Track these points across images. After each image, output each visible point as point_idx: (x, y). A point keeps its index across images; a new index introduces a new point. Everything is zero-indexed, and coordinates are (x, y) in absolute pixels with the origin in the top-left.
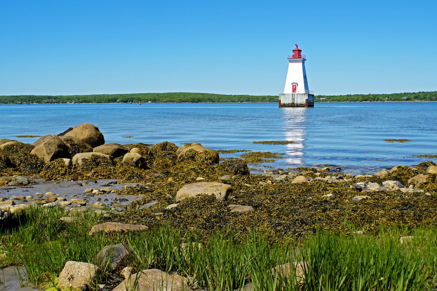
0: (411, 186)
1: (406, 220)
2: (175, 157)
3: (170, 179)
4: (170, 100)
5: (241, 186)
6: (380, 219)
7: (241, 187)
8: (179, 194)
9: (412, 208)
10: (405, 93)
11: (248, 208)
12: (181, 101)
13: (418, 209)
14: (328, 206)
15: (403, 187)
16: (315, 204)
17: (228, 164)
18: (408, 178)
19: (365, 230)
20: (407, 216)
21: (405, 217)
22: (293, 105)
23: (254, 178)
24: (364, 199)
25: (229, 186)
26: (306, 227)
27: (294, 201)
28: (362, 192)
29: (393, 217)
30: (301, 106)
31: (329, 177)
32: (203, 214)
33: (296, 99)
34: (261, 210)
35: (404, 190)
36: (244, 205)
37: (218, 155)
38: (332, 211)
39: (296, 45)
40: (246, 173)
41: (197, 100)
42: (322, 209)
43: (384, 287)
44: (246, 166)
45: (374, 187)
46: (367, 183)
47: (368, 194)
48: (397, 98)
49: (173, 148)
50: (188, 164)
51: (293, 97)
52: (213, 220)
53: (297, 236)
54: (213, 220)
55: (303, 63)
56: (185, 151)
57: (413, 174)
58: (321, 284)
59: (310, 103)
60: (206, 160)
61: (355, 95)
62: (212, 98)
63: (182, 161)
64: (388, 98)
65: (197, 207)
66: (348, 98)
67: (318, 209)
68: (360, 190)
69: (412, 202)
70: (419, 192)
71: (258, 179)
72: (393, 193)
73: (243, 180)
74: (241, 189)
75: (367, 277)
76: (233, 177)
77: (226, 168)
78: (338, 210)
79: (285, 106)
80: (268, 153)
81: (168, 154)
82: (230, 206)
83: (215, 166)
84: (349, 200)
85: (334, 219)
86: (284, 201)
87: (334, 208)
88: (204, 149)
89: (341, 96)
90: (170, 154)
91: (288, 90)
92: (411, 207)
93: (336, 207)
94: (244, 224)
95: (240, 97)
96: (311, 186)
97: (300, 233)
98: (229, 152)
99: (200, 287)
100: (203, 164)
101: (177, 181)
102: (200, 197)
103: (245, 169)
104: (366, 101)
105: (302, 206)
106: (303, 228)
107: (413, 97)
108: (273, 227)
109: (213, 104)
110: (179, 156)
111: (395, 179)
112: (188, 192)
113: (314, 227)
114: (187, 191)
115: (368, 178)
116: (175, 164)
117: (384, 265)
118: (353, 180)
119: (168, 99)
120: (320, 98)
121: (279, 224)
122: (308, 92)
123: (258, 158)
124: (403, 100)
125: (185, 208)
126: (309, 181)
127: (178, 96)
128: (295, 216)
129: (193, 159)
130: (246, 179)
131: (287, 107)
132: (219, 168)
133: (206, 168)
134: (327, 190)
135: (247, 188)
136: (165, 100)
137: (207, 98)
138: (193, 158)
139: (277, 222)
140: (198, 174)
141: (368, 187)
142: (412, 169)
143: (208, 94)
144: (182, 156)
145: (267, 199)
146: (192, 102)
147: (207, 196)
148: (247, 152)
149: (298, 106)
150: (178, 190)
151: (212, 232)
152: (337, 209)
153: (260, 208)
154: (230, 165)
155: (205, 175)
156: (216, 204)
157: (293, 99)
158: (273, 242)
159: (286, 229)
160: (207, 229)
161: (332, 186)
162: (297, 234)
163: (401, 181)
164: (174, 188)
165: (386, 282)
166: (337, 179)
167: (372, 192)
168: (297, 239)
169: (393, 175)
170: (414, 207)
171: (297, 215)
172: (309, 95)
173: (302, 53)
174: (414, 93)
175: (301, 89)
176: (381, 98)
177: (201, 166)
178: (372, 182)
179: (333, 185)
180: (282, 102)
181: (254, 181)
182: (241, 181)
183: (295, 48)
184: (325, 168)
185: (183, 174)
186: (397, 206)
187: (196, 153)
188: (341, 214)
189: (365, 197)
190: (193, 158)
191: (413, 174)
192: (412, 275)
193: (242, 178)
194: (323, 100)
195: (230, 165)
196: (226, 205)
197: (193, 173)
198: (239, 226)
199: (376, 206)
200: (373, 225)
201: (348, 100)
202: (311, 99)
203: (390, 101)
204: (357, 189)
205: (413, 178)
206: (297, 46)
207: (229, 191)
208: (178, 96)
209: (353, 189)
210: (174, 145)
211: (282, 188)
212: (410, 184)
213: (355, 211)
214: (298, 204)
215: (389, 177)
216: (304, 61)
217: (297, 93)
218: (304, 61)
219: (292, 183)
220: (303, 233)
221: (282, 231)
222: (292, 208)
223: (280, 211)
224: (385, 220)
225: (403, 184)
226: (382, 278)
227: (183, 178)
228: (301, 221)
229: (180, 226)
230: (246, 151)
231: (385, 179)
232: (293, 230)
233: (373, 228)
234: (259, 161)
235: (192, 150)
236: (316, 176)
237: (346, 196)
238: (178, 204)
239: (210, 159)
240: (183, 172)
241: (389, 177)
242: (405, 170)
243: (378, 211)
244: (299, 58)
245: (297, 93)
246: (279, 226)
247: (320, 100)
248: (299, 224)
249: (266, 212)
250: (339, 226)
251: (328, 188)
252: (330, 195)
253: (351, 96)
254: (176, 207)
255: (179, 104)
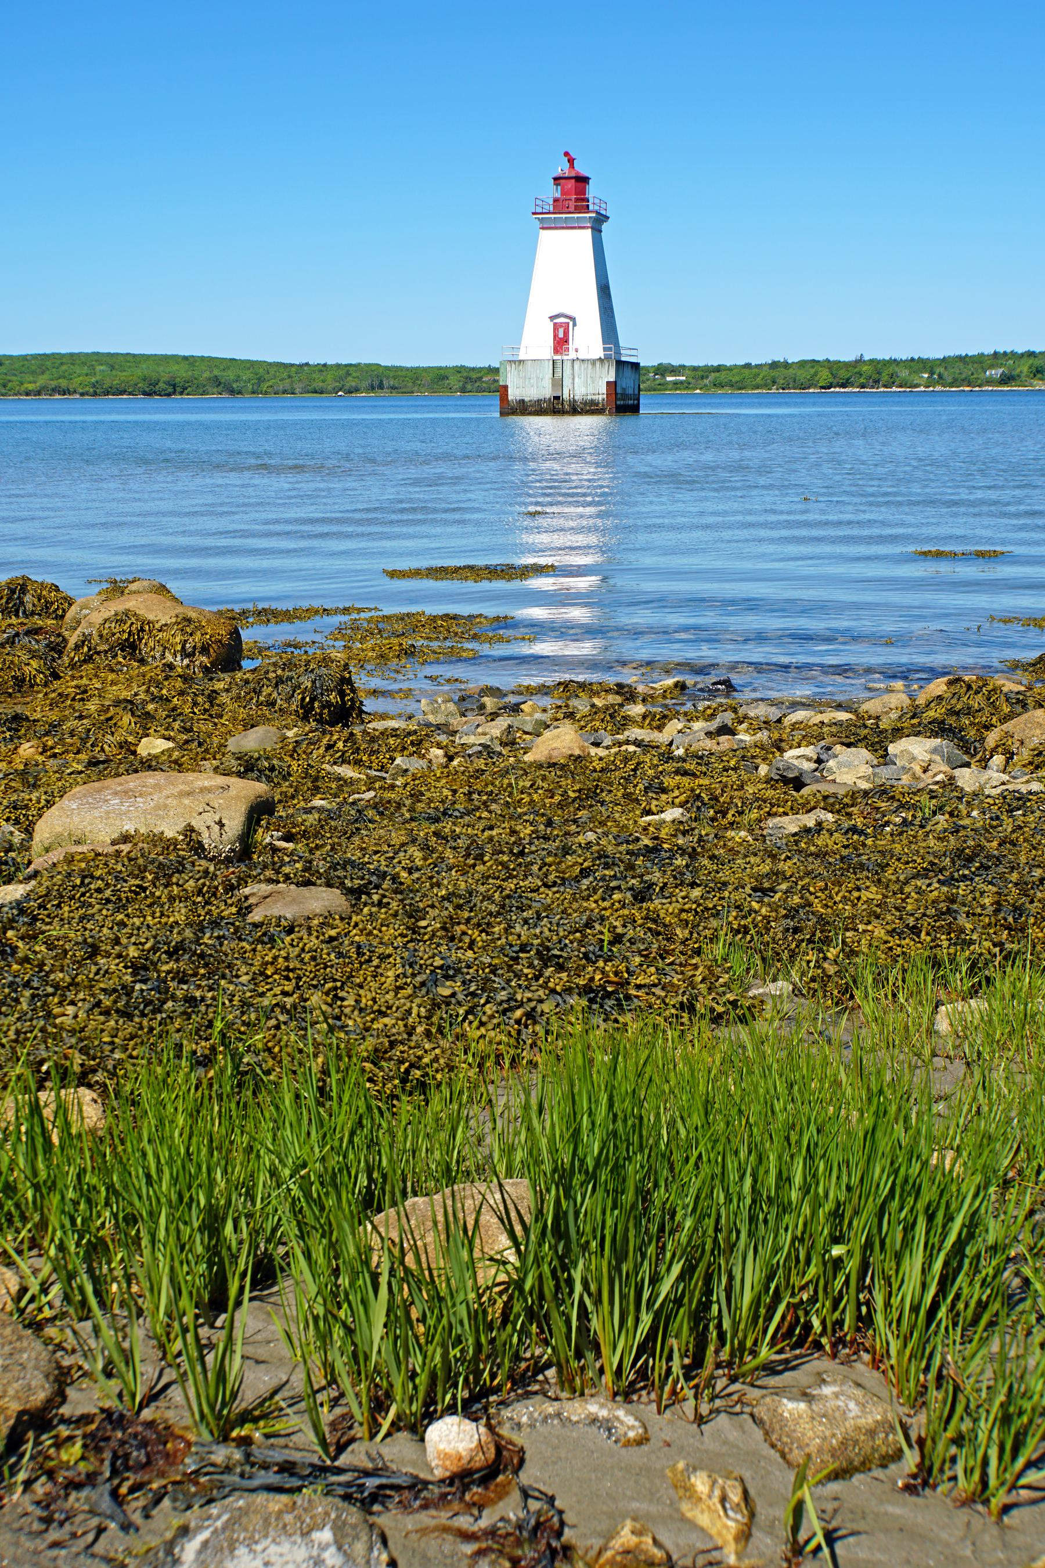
0: (998, 760)
1: (962, 930)
2: (58, 648)
3: (27, 750)
4: (54, 383)
5: (316, 779)
6: (861, 927)
7: (316, 783)
8: (45, 830)
9: (992, 874)
10: (325, 365)
11: (324, 900)
12: (100, 391)
13: (1014, 877)
14: (656, 876)
15: (967, 765)
16: (607, 866)
17: (272, 675)
18: (988, 727)
19: (803, 974)
20: (968, 914)
21: (962, 920)
22: (556, 407)
23: (373, 739)
24: (807, 830)
25: (258, 788)
26: (559, 980)
27: (522, 853)
28: (805, 791)
29: (911, 921)
30: (589, 408)
31: (680, 726)
32: (124, 941)
33: (567, 382)
34: (380, 904)
35: (967, 779)
36: (308, 883)
37: (235, 635)
38: (672, 895)
39: (566, 154)
40: (345, 712)
41: (168, 383)
42: (631, 889)
43: (847, 1282)
44: (349, 681)
45: (851, 769)
46: (829, 749)
47: (828, 802)
48: (966, 373)
49: (54, 604)
50: (111, 676)
51: (558, 375)
52: (165, 968)
53: (518, 1022)
54: (165, 968)
55: (597, 230)
56: (97, 618)
57: (1006, 709)
58: (578, 1288)
59: (625, 396)
60: (188, 656)
61: (803, 364)
62: (230, 375)
63: (88, 659)
64: (932, 373)
65: (108, 901)
66: (774, 373)
67: (619, 888)
68: (798, 783)
69: (995, 844)
70: (1024, 789)
71: (391, 741)
72: (924, 798)
73: (329, 747)
74: (316, 790)
75: (776, 1251)
76: (290, 734)
77: (266, 691)
78: (696, 893)
79: (523, 408)
80: (446, 617)
81: (28, 633)
82: (247, 891)
83: (220, 686)
84: (751, 831)
85: (678, 931)
86: (480, 857)
87: (682, 884)
88: (179, 610)
89: (748, 366)
90: (36, 631)
91: (536, 342)
92: (987, 868)
93: (688, 877)
94: (299, 978)
95: (342, 372)
96: (602, 770)
97: (534, 1009)
98: (288, 616)
99: (72, 1311)
100: (167, 678)
101: (55, 756)
102: (125, 848)
103: (342, 694)
104: (843, 386)
105: (551, 877)
106: (545, 986)
107: (1025, 369)
108: (423, 984)
109: (238, 402)
110: (72, 641)
111: (939, 729)
112: (89, 818)
113: (592, 979)
114: (76, 819)
115: (834, 729)
116: (56, 676)
117: (849, 1188)
118: (776, 736)
119: (42, 381)
120: (663, 375)
121: (449, 972)
122: (618, 352)
123: (407, 640)
124: (989, 382)
125: (59, 906)
126: (597, 744)
127: (86, 370)
128: (518, 928)
129: (132, 655)
130: (340, 745)
131: (530, 414)
132: (235, 691)
133: (182, 693)
134: (664, 791)
135: (340, 788)
136: (31, 387)
137: (207, 375)
138: (130, 647)
139: (438, 962)
140: (145, 721)
141: (830, 770)
142: (1005, 689)
143: (211, 359)
144: (85, 639)
145: (414, 841)
146: (145, 393)
147: (156, 839)
148: (363, 615)
149: (576, 409)
150: (49, 804)
151: (151, 1029)
152: (693, 885)
153: (376, 898)
154: (280, 681)
155: (176, 725)
156: (191, 882)
157: (558, 383)
158: (412, 1066)
159: (473, 994)
160: (130, 1017)
161: (686, 773)
162: (518, 1013)
163: (961, 739)
164: (34, 796)
165: (852, 1265)
166: (709, 734)
167: (842, 792)
168: (519, 1032)
169: (931, 713)
170: (1001, 869)
171: (526, 921)
172: (620, 364)
173: (592, 191)
174: (1031, 354)
175: (588, 340)
176: (904, 373)
177: (159, 685)
178: (848, 745)
179: (691, 766)
180: (513, 395)
181: (373, 752)
182: (321, 751)
183: (562, 168)
184: (670, 682)
185: (81, 726)
186: (932, 864)
187: (145, 627)
188: (707, 909)
189: (810, 820)
190: (130, 647)
191: (1006, 709)
192: (963, 1225)
193: (325, 741)
194: (675, 383)
195: (280, 681)
196: (230, 888)
197: (127, 718)
198: (277, 990)
199: (850, 865)
200: (832, 953)
201: (774, 382)
202: (628, 383)
203: (938, 388)
204: (785, 780)
205: (1004, 727)
206: (571, 161)
207: (259, 811)
208: (86, 370)
209: (768, 780)
210: (57, 589)
211: (486, 778)
212: (994, 751)
213: (765, 892)
214: (535, 868)
215: (911, 721)
216: (598, 223)
217: (572, 355)
218: (598, 223)
219: (528, 758)
220: (546, 1007)
221: (459, 1003)
222: (511, 885)
223: (459, 907)
224: (880, 933)
225: (967, 752)
226: (837, 1251)
227: (84, 741)
228: (538, 952)
229: (17, 1001)
230: (360, 610)
231: (897, 733)
232: (503, 995)
233: (831, 970)
234: (410, 652)
235: (127, 613)
236: (627, 721)
237: (741, 813)
238: (33, 883)
239: (205, 650)
240: (81, 717)
241: (915, 721)
242: (977, 693)
243: (858, 889)
244: (578, 210)
245: (572, 355)
246: (447, 977)
247: (664, 385)
248: (531, 966)
249: (395, 915)
250: (696, 967)
251: (668, 781)
252: (673, 814)
253: (786, 365)
254: (18, 903)
255: (89, 402)
